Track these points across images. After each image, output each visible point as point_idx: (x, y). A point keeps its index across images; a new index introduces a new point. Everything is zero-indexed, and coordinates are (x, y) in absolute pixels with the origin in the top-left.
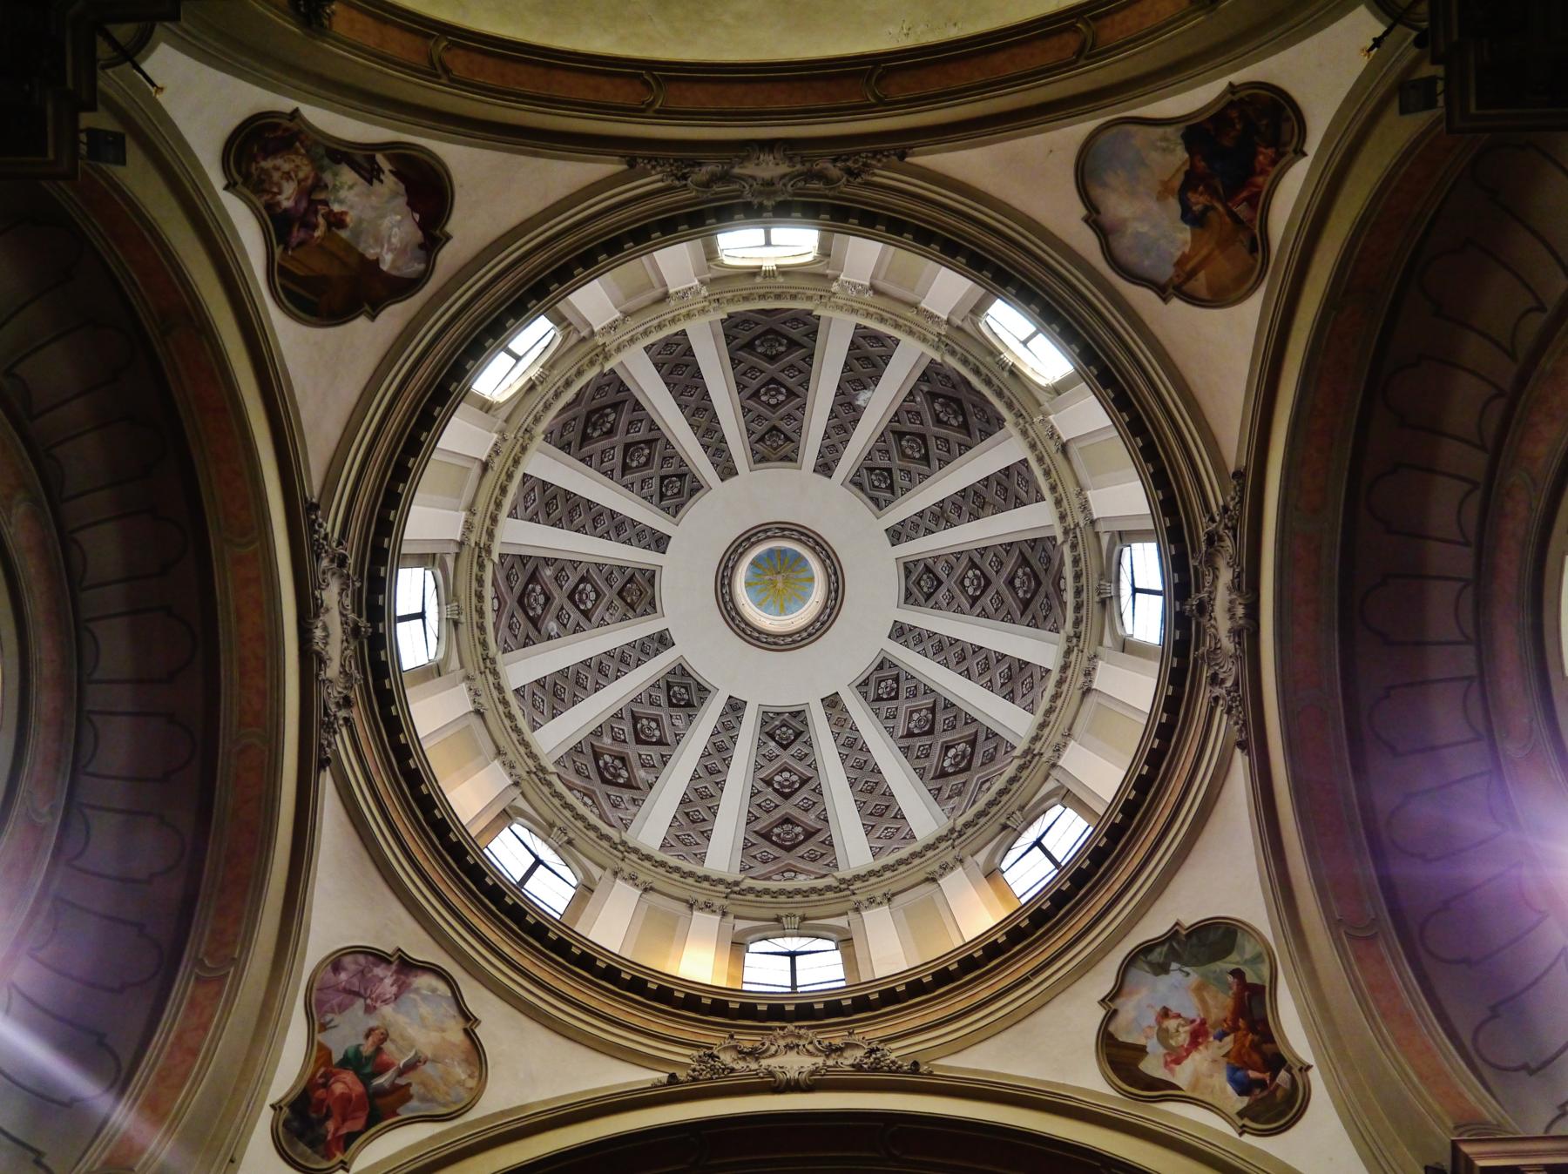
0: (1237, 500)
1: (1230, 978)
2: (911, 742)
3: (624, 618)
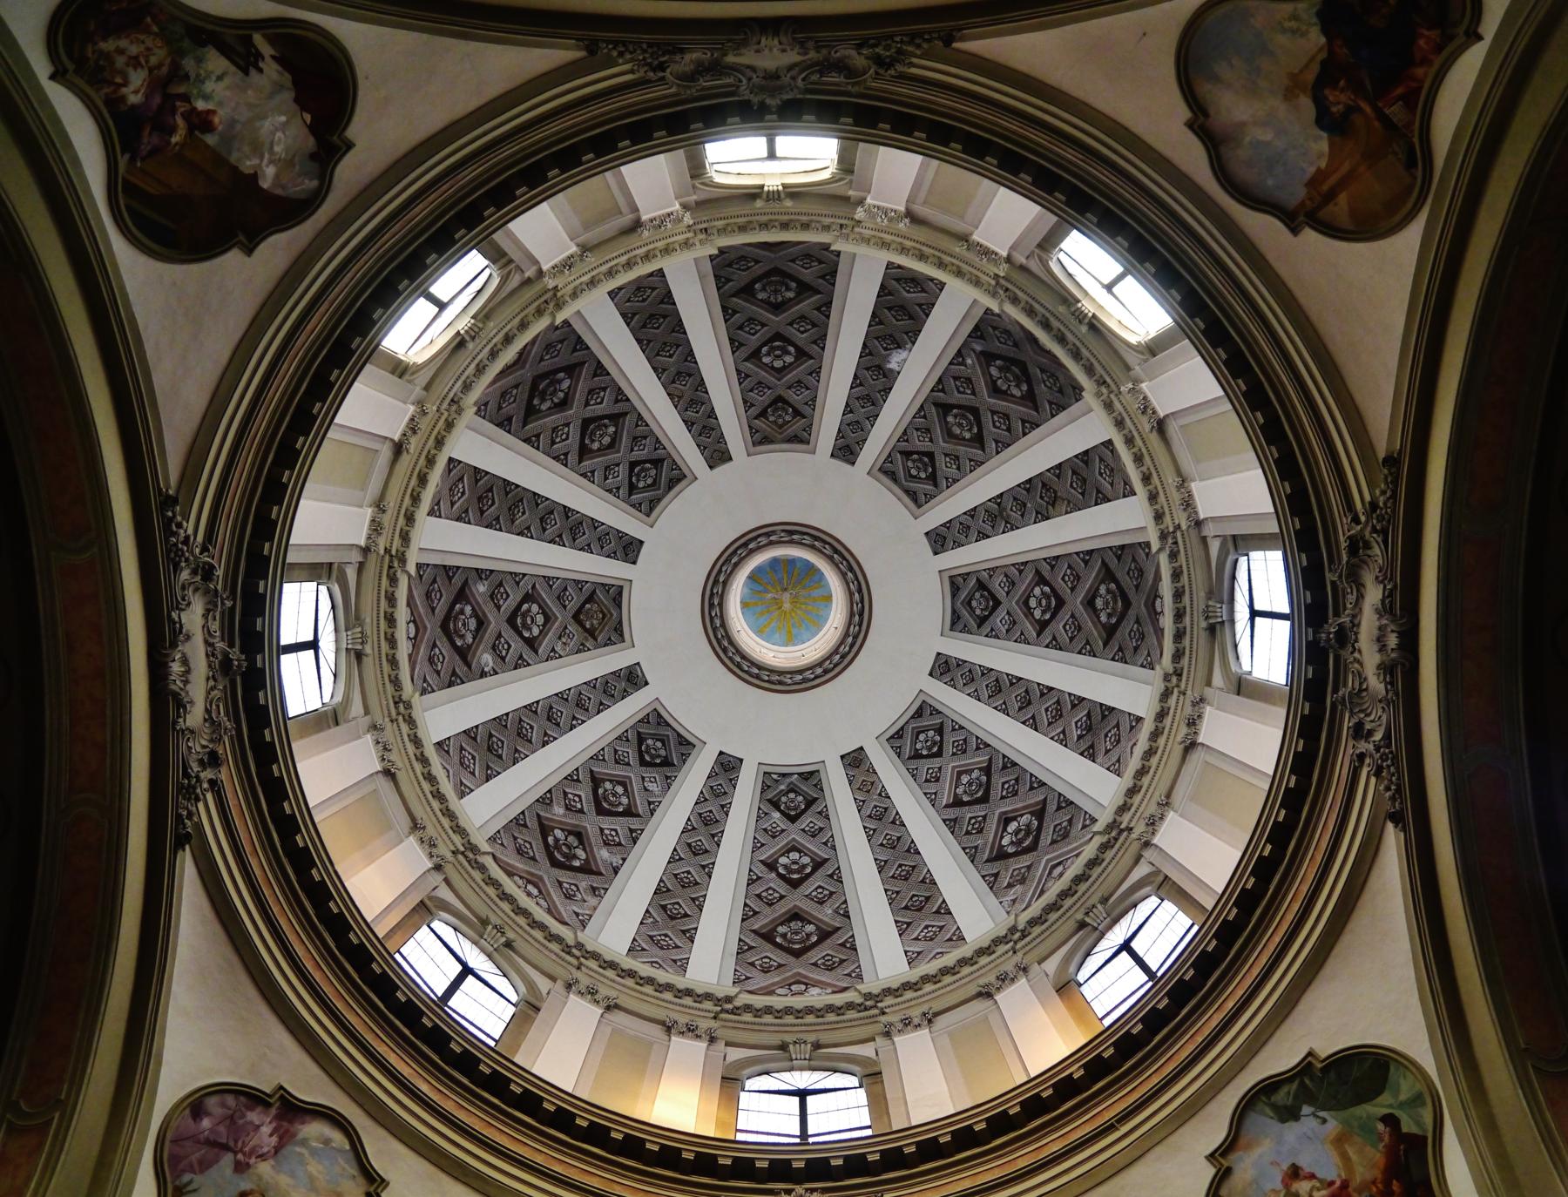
1: (1381, 1127)
3: (581, 649)
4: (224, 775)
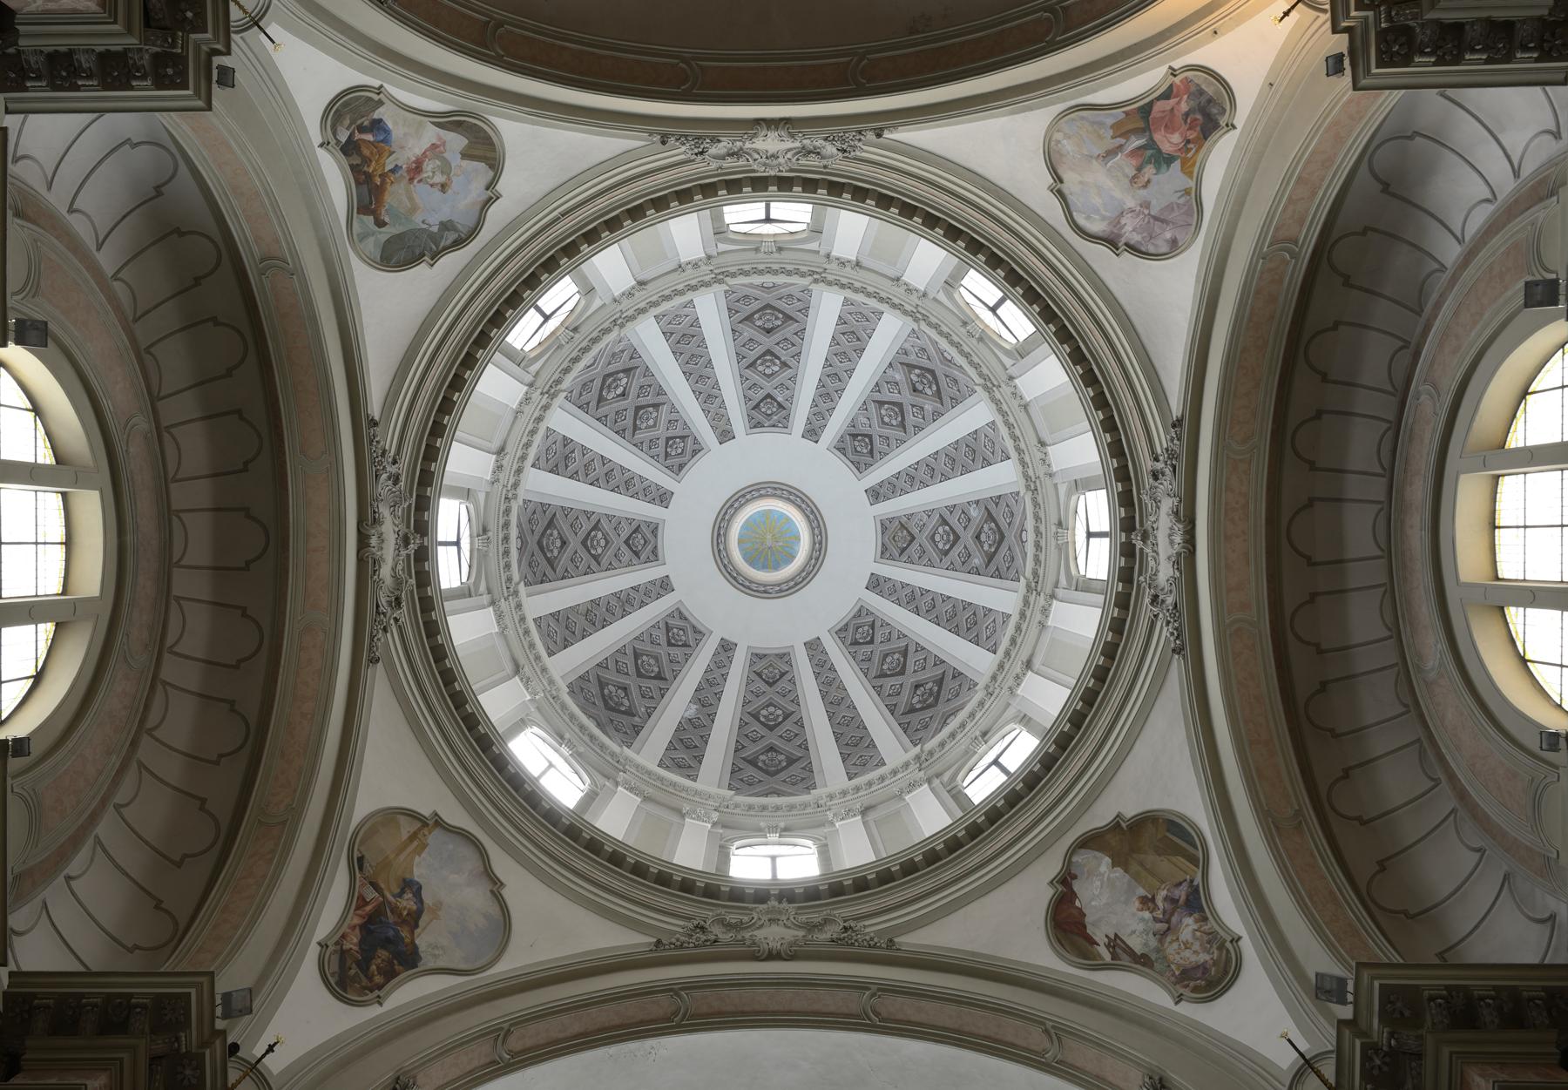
0: (375, 639)
1: (387, 219)
2: (654, 400)
3: (910, 517)
4: (1149, 463)
